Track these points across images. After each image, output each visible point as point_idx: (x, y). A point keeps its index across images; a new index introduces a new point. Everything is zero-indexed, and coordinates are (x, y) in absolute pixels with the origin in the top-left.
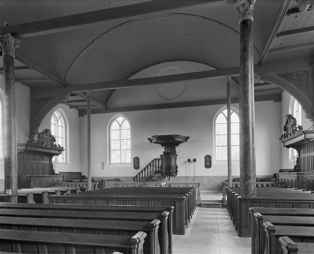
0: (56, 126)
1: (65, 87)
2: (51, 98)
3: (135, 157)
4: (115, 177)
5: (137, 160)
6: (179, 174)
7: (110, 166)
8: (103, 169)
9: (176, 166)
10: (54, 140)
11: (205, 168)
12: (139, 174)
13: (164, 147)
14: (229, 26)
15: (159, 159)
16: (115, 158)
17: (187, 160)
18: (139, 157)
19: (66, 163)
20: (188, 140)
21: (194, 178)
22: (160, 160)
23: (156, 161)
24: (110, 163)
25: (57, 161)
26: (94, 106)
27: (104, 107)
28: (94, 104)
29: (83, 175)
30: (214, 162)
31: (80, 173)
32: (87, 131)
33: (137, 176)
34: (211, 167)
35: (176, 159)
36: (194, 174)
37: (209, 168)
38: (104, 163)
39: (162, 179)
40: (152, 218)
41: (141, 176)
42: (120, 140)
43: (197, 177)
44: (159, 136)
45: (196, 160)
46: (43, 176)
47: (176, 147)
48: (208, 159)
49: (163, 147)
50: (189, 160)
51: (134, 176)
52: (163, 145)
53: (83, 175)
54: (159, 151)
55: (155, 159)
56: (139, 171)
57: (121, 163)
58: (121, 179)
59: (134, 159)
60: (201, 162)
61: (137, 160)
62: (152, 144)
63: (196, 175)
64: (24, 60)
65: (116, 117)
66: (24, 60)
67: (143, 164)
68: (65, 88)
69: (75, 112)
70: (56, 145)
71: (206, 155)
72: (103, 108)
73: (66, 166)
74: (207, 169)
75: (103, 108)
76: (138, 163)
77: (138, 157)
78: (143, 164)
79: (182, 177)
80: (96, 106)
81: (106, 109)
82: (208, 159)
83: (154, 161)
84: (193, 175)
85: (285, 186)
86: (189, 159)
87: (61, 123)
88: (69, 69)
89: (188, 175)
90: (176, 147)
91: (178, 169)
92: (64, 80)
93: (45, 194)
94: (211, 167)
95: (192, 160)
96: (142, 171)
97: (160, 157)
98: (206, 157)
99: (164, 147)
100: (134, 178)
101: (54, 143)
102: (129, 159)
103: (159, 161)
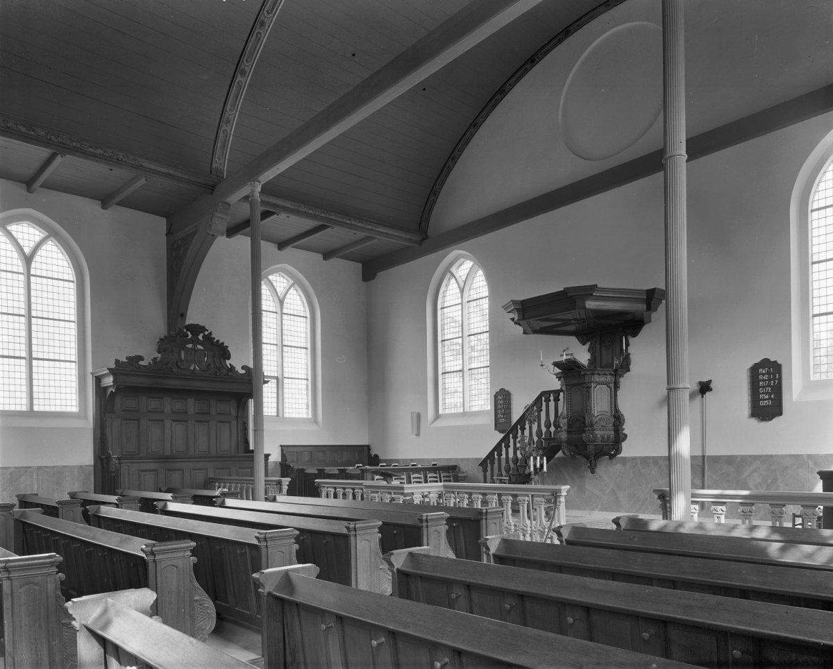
0: (279, 316)
1: (213, 190)
2: (194, 234)
4: (434, 460)
5: (768, 373)
6: (629, 450)
7: (439, 423)
8: (418, 435)
9: (614, 417)
10: (224, 353)
11: (754, 421)
15: (556, 393)
16: (451, 402)
19: (315, 419)
21: (701, 464)
23: (548, 401)
24: (437, 416)
25: (280, 415)
26: (368, 238)
27: (408, 237)
28: (380, 239)
29: (373, 453)
30: (794, 389)
31: (366, 448)
34: (779, 412)
35: (617, 386)
37: (771, 419)
38: (419, 416)
40: (159, 590)
42: (462, 337)
43: (716, 459)
44: (523, 302)
45: (712, 385)
47: (631, 340)
48: (766, 377)
51: (484, 456)
53: (373, 453)
57: (464, 414)
58: (463, 467)
60: (734, 395)
61: (768, 373)
63: (711, 451)
64: (24, 130)
65: (451, 264)
66: (24, 130)
68: (212, 193)
69: (346, 270)
70: (232, 368)
71: (758, 360)
72: (411, 240)
73: (313, 427)
74: (764, 424)
75: (411, 240)
77: (776, 420)
79: (653, 458)
80: (373, 238)
81: (420, 244)
82: (764, 380)
86: (705, 380)
87: (296, 301)
88: (221, 134)
90: (631, 340)
91: (627, 428)
92: (209, 171)
93: (490, 522)
94: (780, 414)
98: (754, 370)
99: (587, 346)
100: (483, 464)
101: (228, 362)
102: (482, 402)
103: (557, 400)
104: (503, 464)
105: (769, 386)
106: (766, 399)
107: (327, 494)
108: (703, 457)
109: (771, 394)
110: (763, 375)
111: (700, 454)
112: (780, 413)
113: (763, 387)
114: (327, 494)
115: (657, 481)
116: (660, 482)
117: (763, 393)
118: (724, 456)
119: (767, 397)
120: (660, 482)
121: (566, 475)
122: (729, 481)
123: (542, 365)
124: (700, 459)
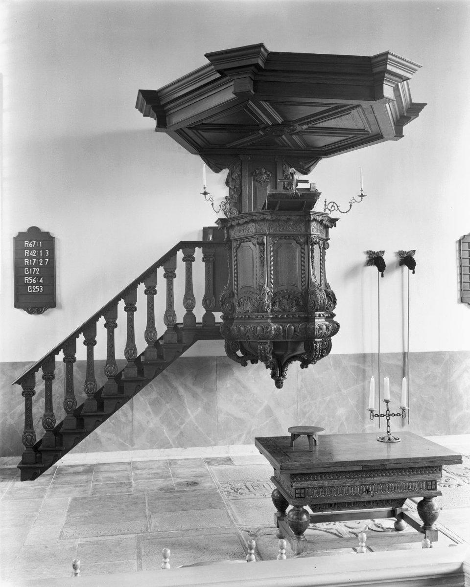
3: (24, 229)
5: (37, 248)
12: (68, 345)
13: (225, 173)
14: (402, 342)
17: (364, 258)
18: (54, 232)
20: (406, 129)
21: (400, 363)
22: (198, 253)
23: (189, 259)
32: (391, 108)
33: (48, 362)
36: (405, 336)
39: (214, 378)
41: (81, 353)
43: (421, 357)
46: (347, 139)
49: (217, 169)
50: (376, 260)
52: (214, 157)
54: (192, 199)
55: (182, 245)
56: (57, 326)
59: (20, 240)
61: (37, 248)
62: (163, 135)
67: (82, 287)
76: (48, 274)
78: (82, 287)
82: (30, 257)
83: (180, 254)
84: (399, 350)
85: (405, 82)
89: (370, 348)
95: (389, 258)
96: (88, 329)
97: (198, 238)
99: (225, 173)
104: (79, 376)
105: (37, 265)
106: (33, 285)
107: (85, 491)
108: (404, 354)
109: (39, 277)
110: (30, 249)
111: (400, 350)
112: (17, 305)
113: (30, 267)
114: (85, 491)
115: (339, 390)
116: (344, 391)
117: (29, 276)
118: (429, 352)
119: (34, 281)
120: (344, 391)
121: (181, 390)
122: (435, 386)
123: (205, 193)
124: (401, 357)
